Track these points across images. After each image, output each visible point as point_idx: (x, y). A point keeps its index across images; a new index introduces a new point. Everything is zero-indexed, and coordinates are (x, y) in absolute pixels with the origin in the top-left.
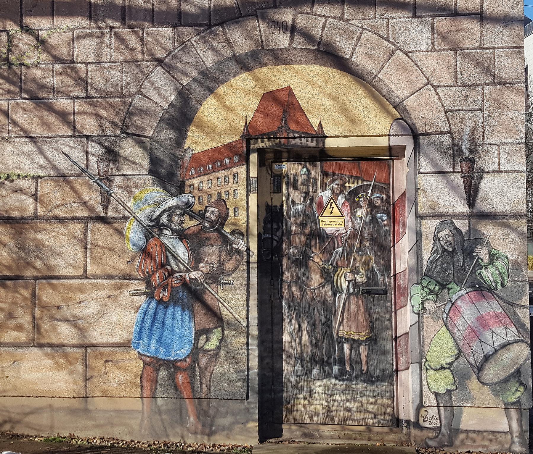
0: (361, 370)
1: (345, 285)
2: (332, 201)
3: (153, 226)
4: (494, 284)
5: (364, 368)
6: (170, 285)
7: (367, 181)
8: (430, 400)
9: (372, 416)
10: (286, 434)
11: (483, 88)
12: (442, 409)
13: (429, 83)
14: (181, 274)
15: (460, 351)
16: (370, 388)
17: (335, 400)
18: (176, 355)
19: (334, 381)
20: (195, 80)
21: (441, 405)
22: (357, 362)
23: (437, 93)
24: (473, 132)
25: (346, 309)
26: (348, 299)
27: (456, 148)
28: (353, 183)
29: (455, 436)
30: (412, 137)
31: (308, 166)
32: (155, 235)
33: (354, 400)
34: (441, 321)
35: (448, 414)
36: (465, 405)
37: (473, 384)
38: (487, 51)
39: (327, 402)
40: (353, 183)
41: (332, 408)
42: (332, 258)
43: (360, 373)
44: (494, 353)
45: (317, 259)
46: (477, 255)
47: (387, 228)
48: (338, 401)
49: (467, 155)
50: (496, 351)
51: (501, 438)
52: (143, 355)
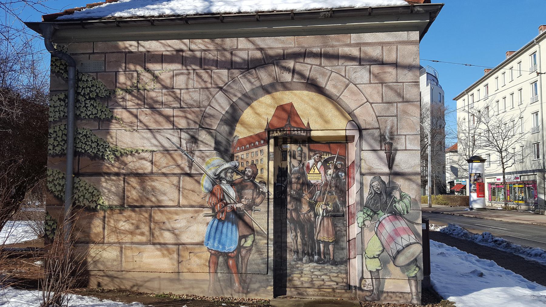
0: (330, 259)
1: (321, 212)
2: (314, 165)
3: (216, 179)
4: (402, 212)
5: (332, 257)
6: (225, 211)
7: (333, 154)
8: (367, 275)
9: (335, 284)
10: (288, 293)
11: (397, 104)
12: (374, 280)
13: (368, 101)
14: (231, 205)
15: (384, 248)
16: (334, 268)
17: (316, 275)
18: (228, 250)
19: (315, 264)
20: (240, 98)
24: (392, 128)
26: (323, 219)
28: (326, 156)
29: (381, 295)
30: (358, 131)
31: (302, 146)
32: (217, 183)
33: (326, 274)
34: (374, 231)
35: (377, 282)
37: (391, 266)
39: (311, 276)
40: (326, 156)
41: (313, 279)
44: (402, 249)
46: (394, 196)
47: (344, 180)
48: (317, 275)
49: (388, 140)
50: (404, 248)
52: (210, 249)
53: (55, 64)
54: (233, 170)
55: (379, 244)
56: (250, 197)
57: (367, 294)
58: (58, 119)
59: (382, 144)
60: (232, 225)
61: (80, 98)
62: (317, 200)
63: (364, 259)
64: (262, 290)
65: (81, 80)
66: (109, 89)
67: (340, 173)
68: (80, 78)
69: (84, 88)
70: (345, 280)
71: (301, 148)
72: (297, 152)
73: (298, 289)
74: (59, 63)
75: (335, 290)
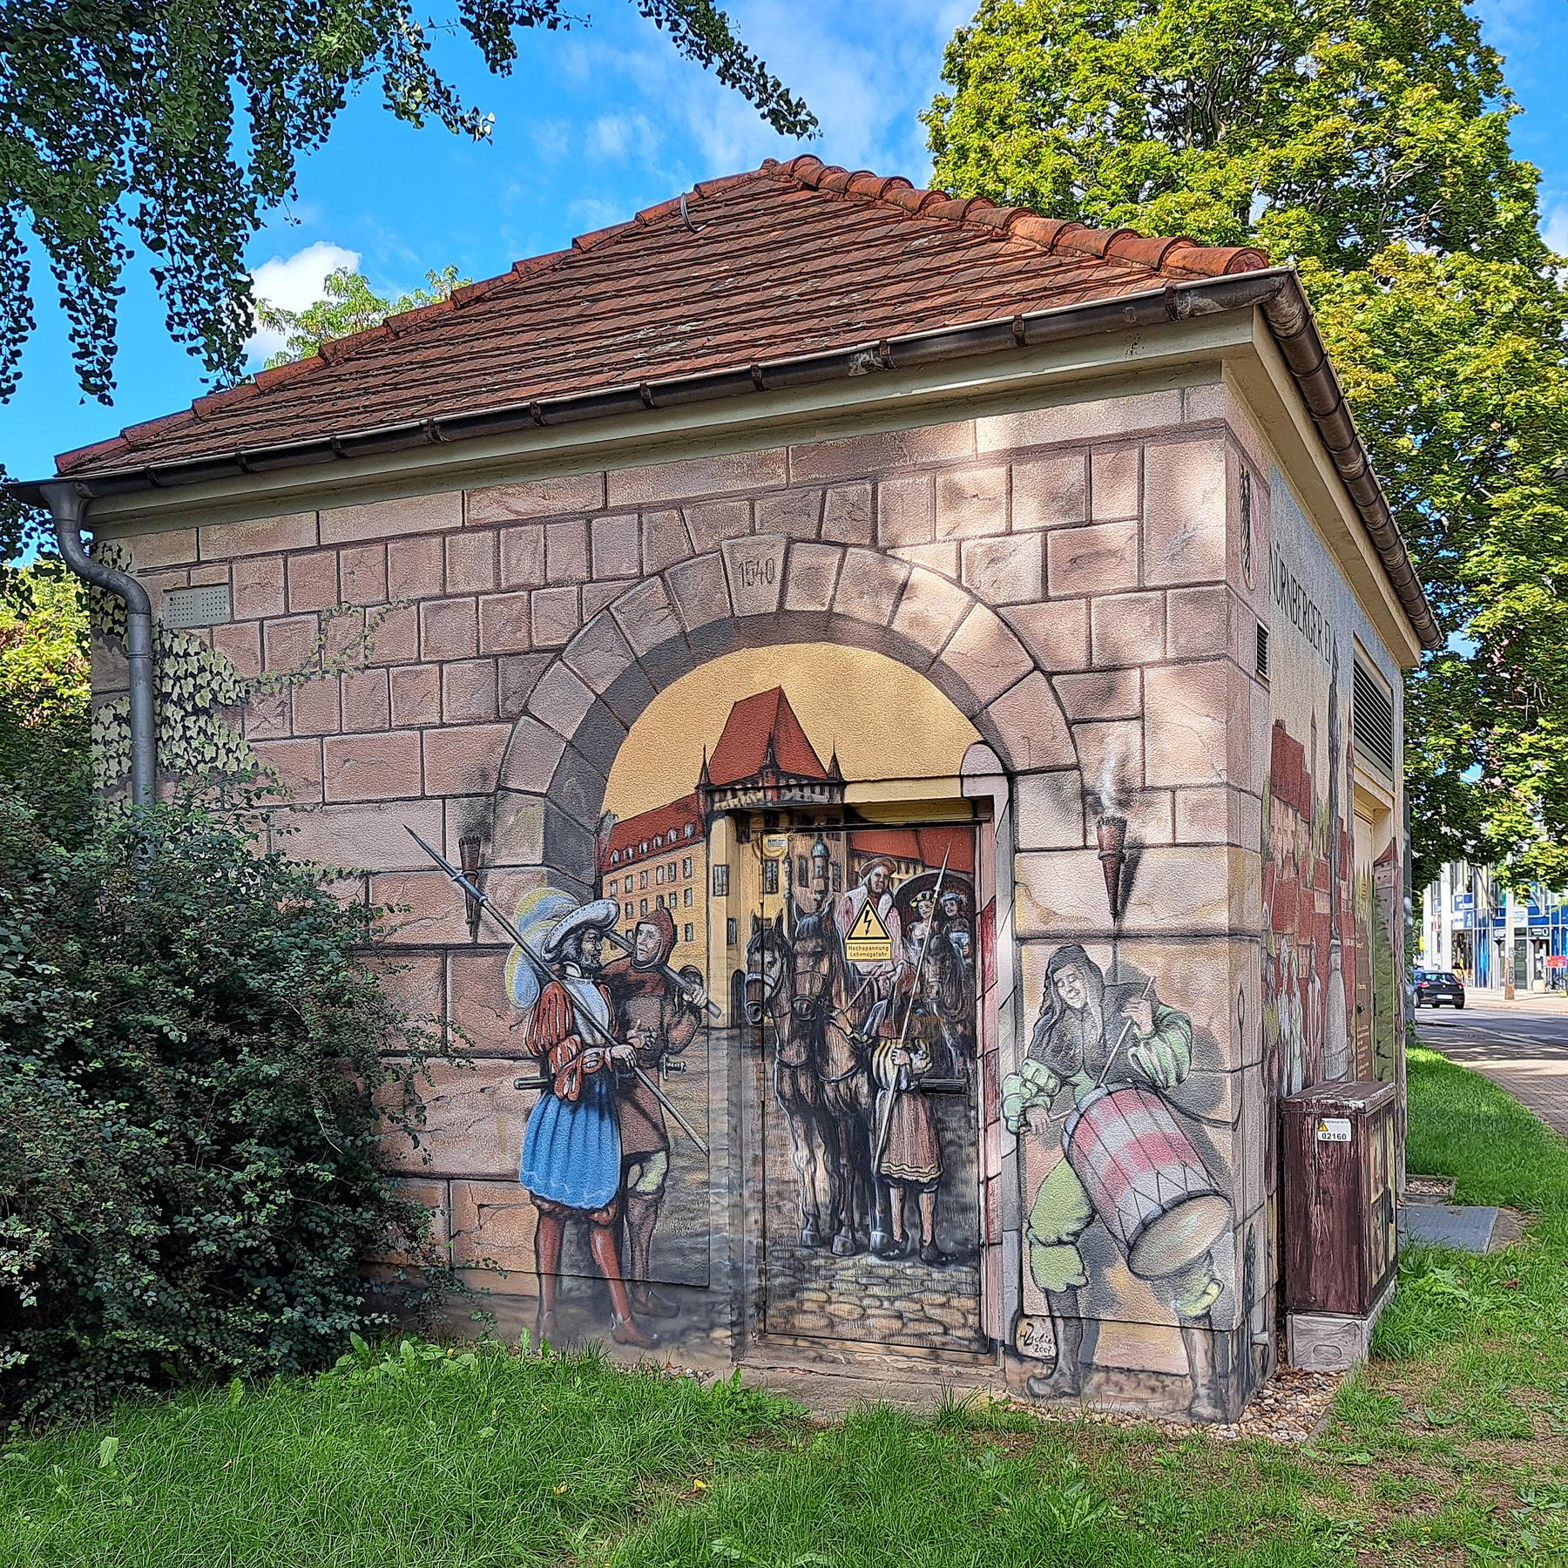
0: (922, 1241)
1: (892, 1076)
2: (868, 908)
3: (552, 960)
4: (1161, 1077)
5: (927, 1237)
6: (579, 1071)
7: (933, 867)
8: (1036, 1303)
9: (940, 1330)
11: (1142, 673)
12: (1060, 1322)
13: (1037, 667)
14: (595, 1050)
15: (1094, 1211)
16: (936, 1275)
17: (873, 1296)
18: (591, 1200)
19: (873, 1260)
21: (1057, 1314)
22: (914, 1225)
23: (1053, 689)
24: (1123, 762)
25: (895, 1121)
26: (898, 1100)
27: (1090, 799)
28: (907, 872)
29: (1085, 1377)
30: (1005, 778)
31: (826, 840)
32: (554, 977)
33: (908, 1297)
34: (1059, 1148)
35: (1072, 1332)
36: (1102, 1317)
38: (1150, 594)
39: (861, 1299)
40: (907, 872)
41: (869, 1312)
42: (870, 1020)
43: (918, 1246)
44: (1160, 1216)
45: (842, 1022)
46: (1130, 1017)
47: (969, 961)
48: (878, 1298)
49: (1111, 811)
50: (1165, 1211)
51: (1173, 1385)
52: (538, 1197)
53: (102, 608)
54: (601, 932)
55: (1077, 1193)
56: (653, 1023)
57: (1037, 1371)
58: (115, 782)
59: (1088, 824)
60: (601, 1117)
61: (170, 710)
62: (877, 1031)
63: (1026, 1245)
64: (694, 1339)
65: (168, 653)
66: (246, 676)
67: (953, 935)
68: (167, 646)
69: (179, 679)
70: (972, 1320)
71: (826, 848)
72: (810, 863)
73: (819, 1343)
74: (112, 604)
75: (940, 1352)
